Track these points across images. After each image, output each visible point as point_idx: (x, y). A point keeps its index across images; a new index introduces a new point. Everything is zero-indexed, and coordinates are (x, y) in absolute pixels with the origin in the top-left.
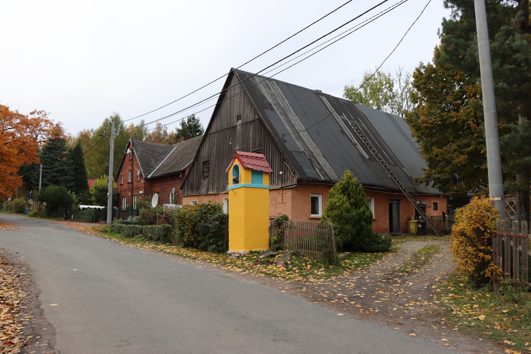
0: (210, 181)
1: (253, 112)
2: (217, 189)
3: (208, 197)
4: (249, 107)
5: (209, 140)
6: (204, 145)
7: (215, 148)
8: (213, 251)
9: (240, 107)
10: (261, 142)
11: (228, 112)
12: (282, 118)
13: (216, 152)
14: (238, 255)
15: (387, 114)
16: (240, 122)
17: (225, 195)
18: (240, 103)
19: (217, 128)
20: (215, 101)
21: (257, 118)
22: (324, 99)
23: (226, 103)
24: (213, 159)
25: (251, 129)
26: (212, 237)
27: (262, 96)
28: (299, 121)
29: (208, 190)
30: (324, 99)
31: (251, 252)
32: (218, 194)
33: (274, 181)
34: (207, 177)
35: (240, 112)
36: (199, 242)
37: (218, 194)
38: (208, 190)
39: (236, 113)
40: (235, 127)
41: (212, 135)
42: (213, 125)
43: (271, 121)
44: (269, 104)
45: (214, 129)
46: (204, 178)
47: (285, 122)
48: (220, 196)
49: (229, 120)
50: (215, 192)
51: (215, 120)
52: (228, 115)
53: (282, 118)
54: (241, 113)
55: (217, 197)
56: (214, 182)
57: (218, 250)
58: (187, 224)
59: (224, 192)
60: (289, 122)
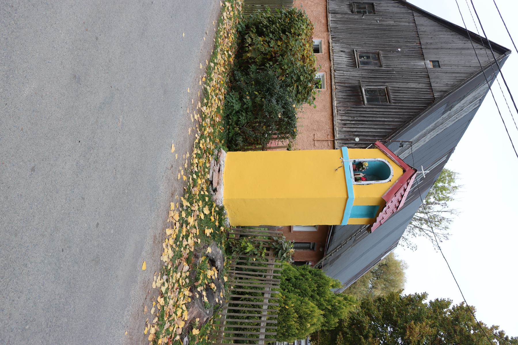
0: (346, 16)
1: (444, 88)
2: (336, 28)
3: (324, 14)
4: (451, 82)
5: (403, 13)
6: (397, 5)
7: (392, 23)
8: (228, 106)
9: (451, 65)
10: (400, 101)
11: (445, 46)
12: (430, 127)
13: (387, 25)
14: (215, 184)
15: (414, 214)
16: (430, 65)
17: (326, 41)
18: (458, 66)
19: (422, 25)
20: (461, 24)
21: (436, 95)
22: (444, 159)
23: (459, 42)
24: (376, 20)
25: (420, 86)
26: (253, 100)
27: (464, 97)
28: (423, 144)
29: (334, 13)
30: (444, 159)
31: (222, 209)
32: (328, 31)
33: (345, 124)
34: (352, 11)
35: (444, 65)
36: (245, 71)
37: (328, 31)
38: (334, 13)
39: (444, 58)
40: (422, 57)
41: (411, 18)
42: (425, 19)
43: (429, 116)
44: (451, 108)
45: (420, 20)
46: (350, 5)
47: (424, 131)
48: (325, 34)
49: (433, 46)
50: (331, 24)
51: (432, 23)
52: (439, 46)
53: (430, 127)
54: (444, 68)
55: (323, 28)
56: (344, 22)
57: (231, 113)
58: (279, 43)
59: (331, 41)
60: (425, 135)
